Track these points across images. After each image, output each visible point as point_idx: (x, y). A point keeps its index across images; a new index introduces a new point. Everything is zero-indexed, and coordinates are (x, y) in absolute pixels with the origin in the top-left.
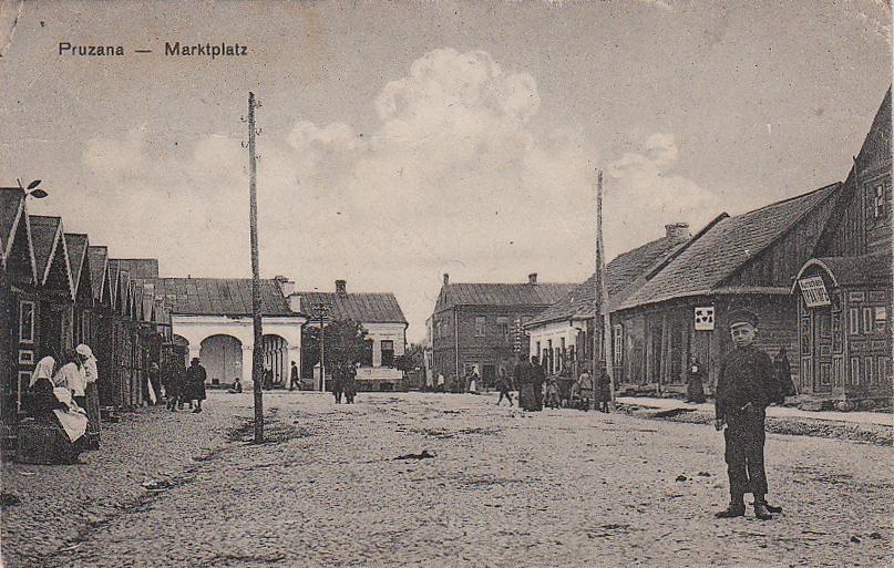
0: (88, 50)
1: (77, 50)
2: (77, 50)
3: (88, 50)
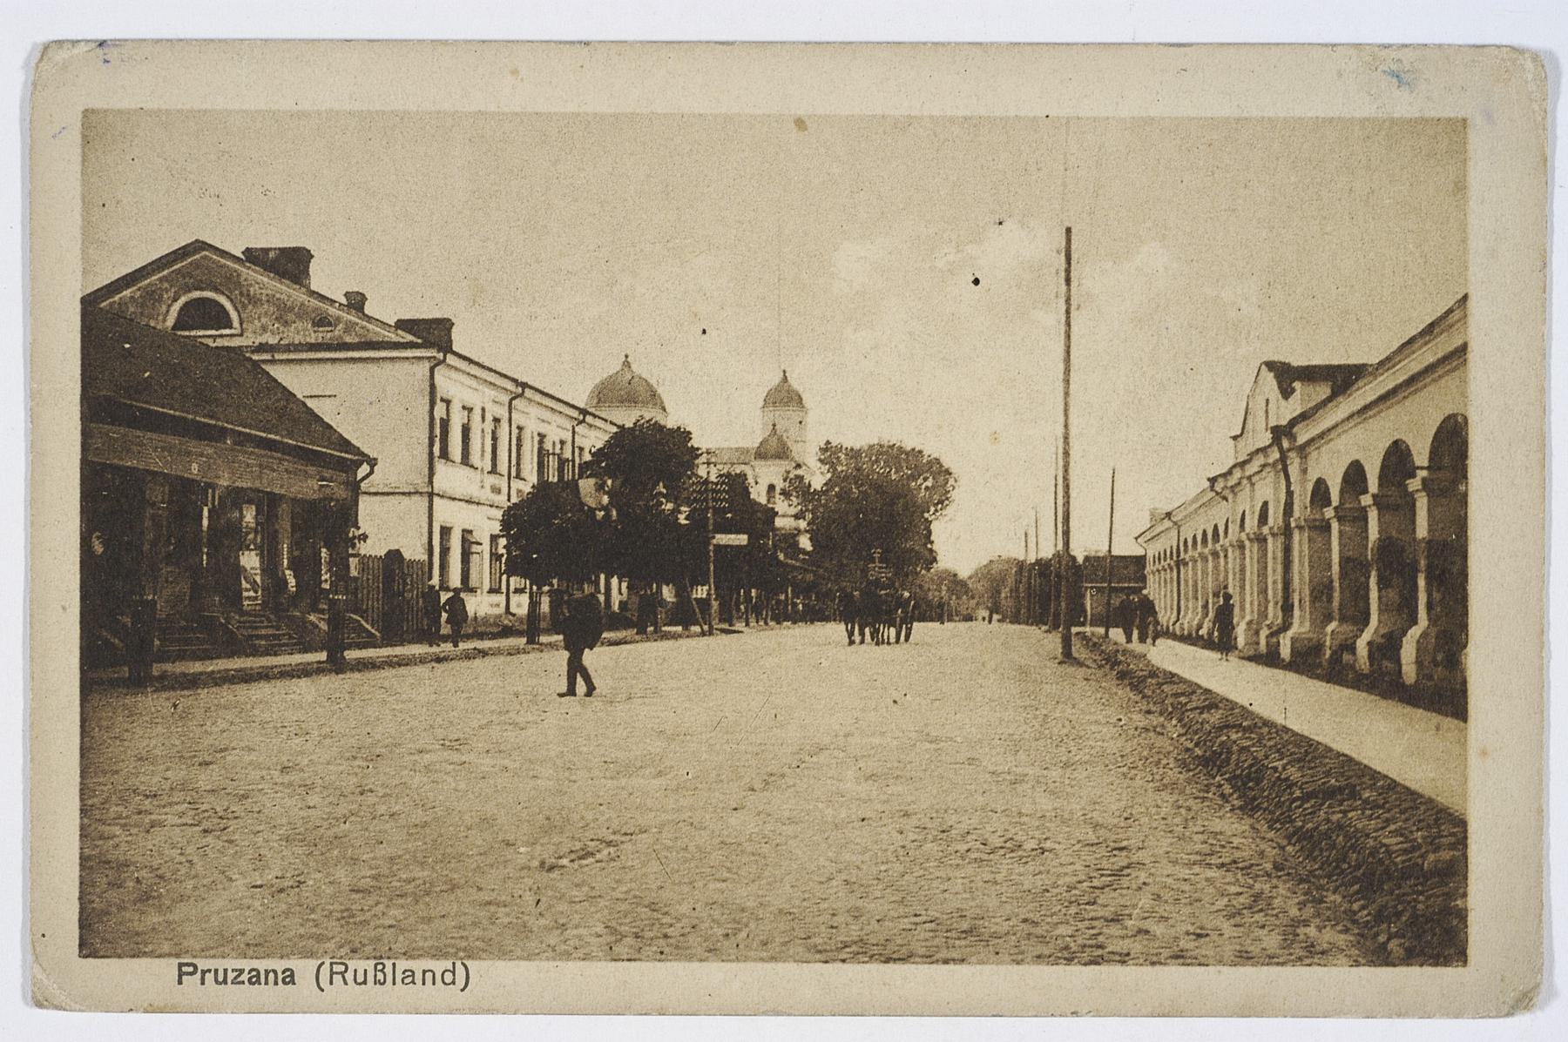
0: (231, 976)
1: (210, 977)
2: (210, 977)
3: (231, 976)
